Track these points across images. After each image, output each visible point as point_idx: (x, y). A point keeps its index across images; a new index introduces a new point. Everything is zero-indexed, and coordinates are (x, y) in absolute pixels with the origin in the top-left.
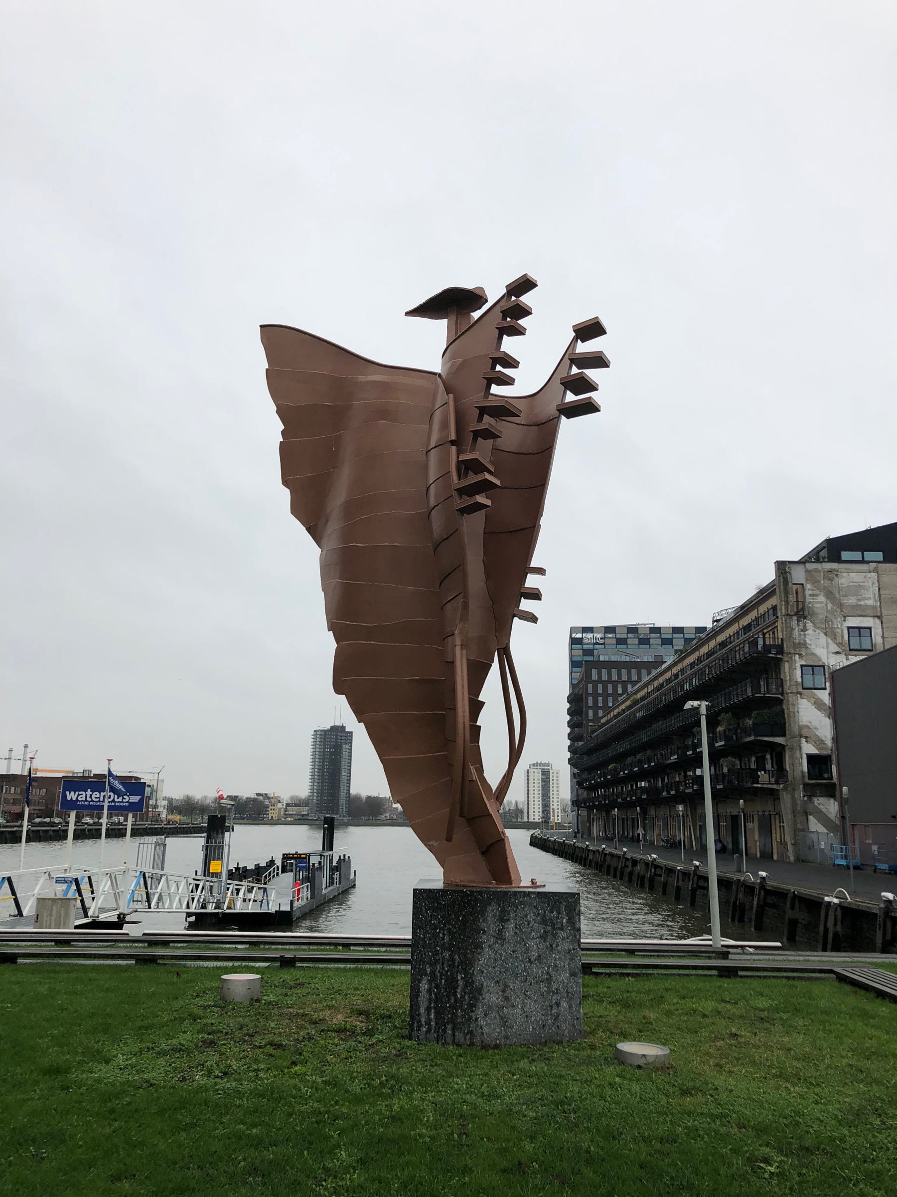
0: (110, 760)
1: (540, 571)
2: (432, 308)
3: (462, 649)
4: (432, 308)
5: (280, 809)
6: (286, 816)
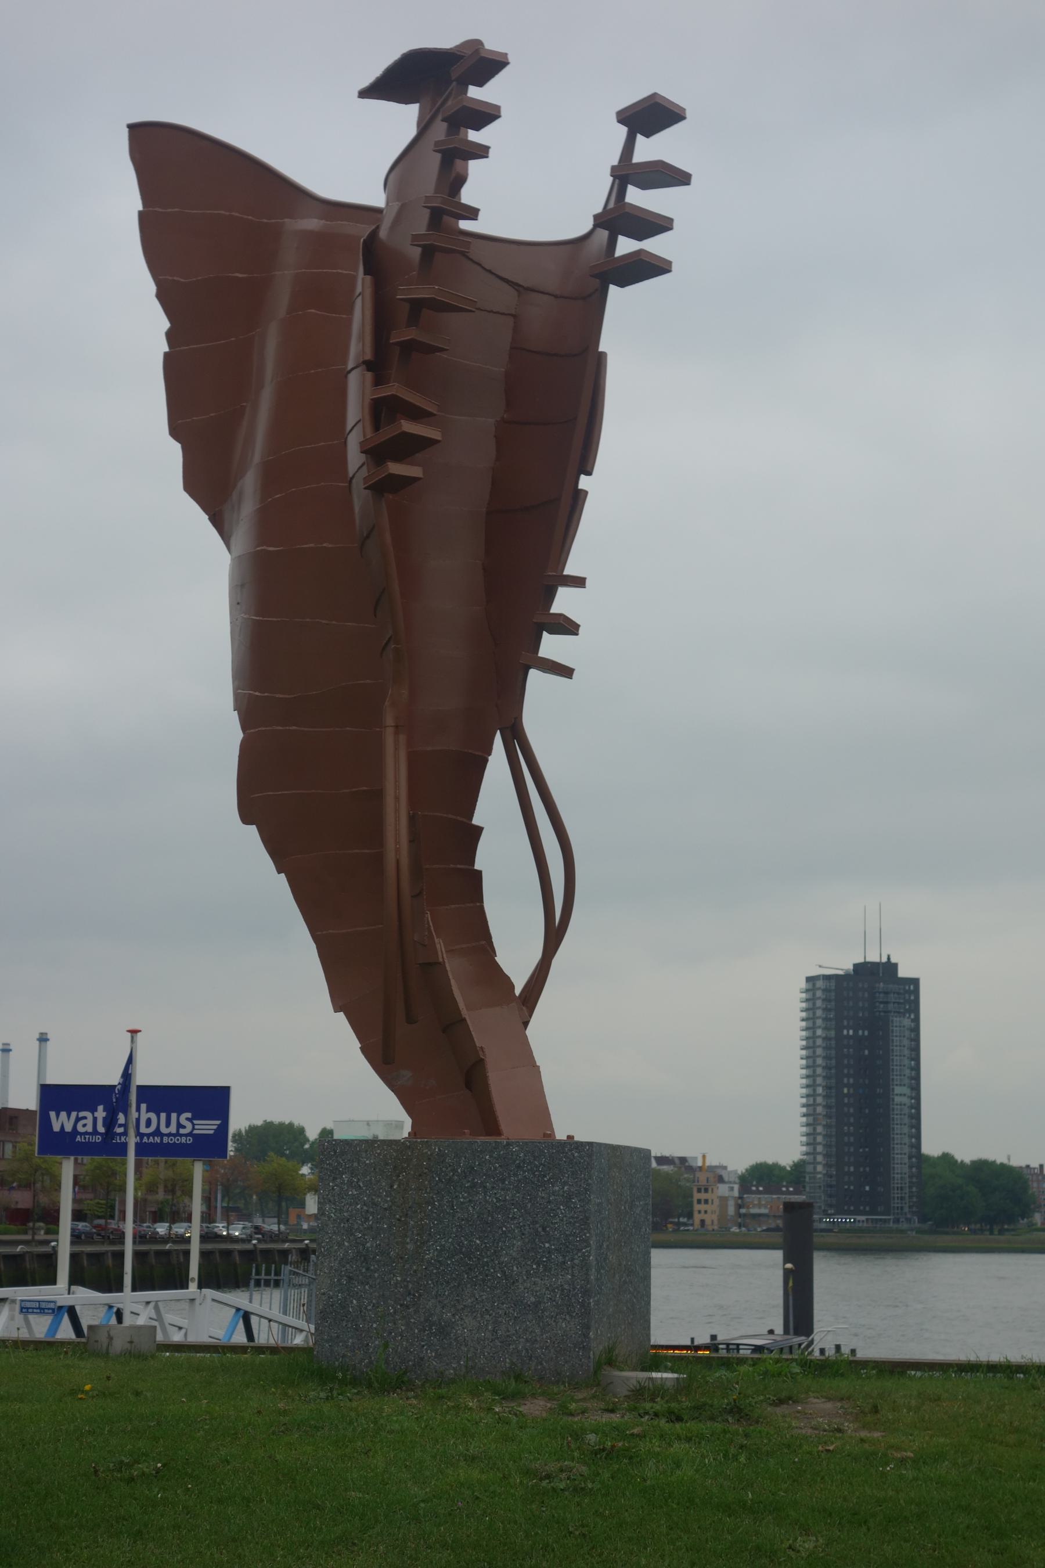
0: (134, 1032)
1: (579, 582)
2: (390, 86)
3: (396, 733)
4: (390, 86)
5: (724, 1200)
6: (744, 1219)
